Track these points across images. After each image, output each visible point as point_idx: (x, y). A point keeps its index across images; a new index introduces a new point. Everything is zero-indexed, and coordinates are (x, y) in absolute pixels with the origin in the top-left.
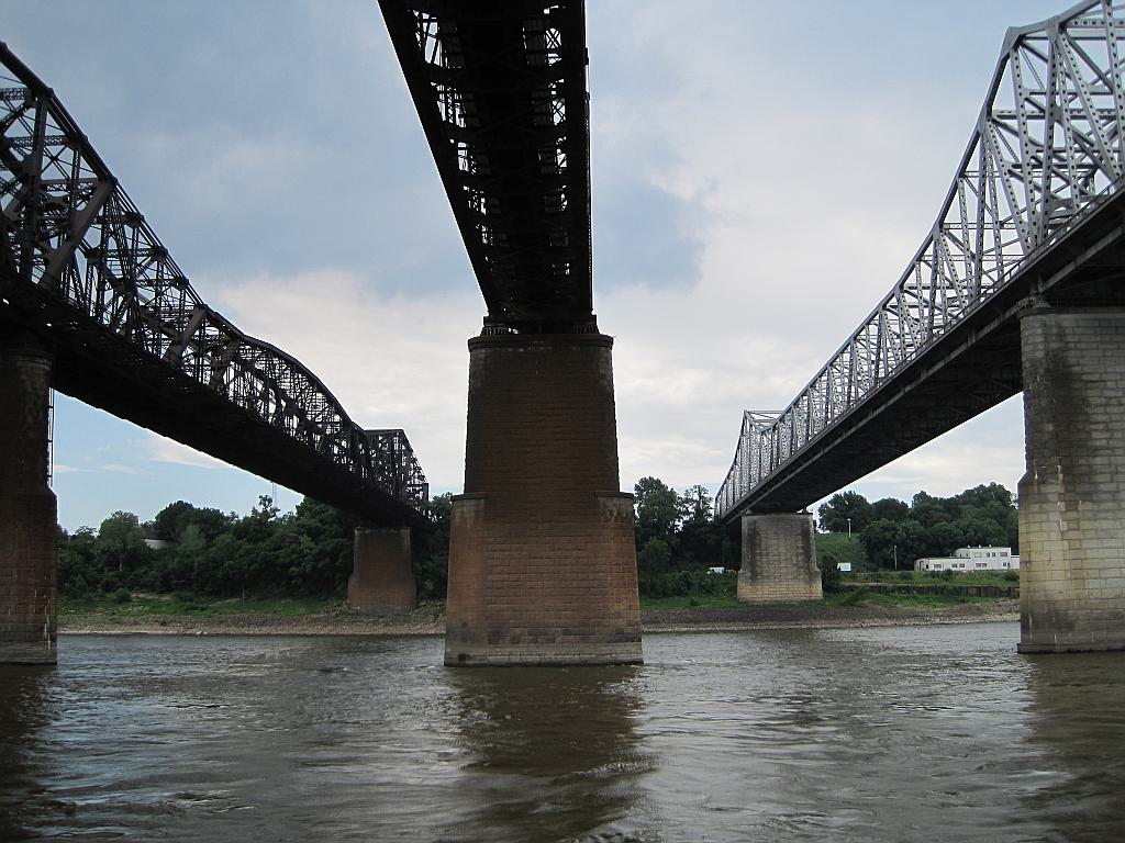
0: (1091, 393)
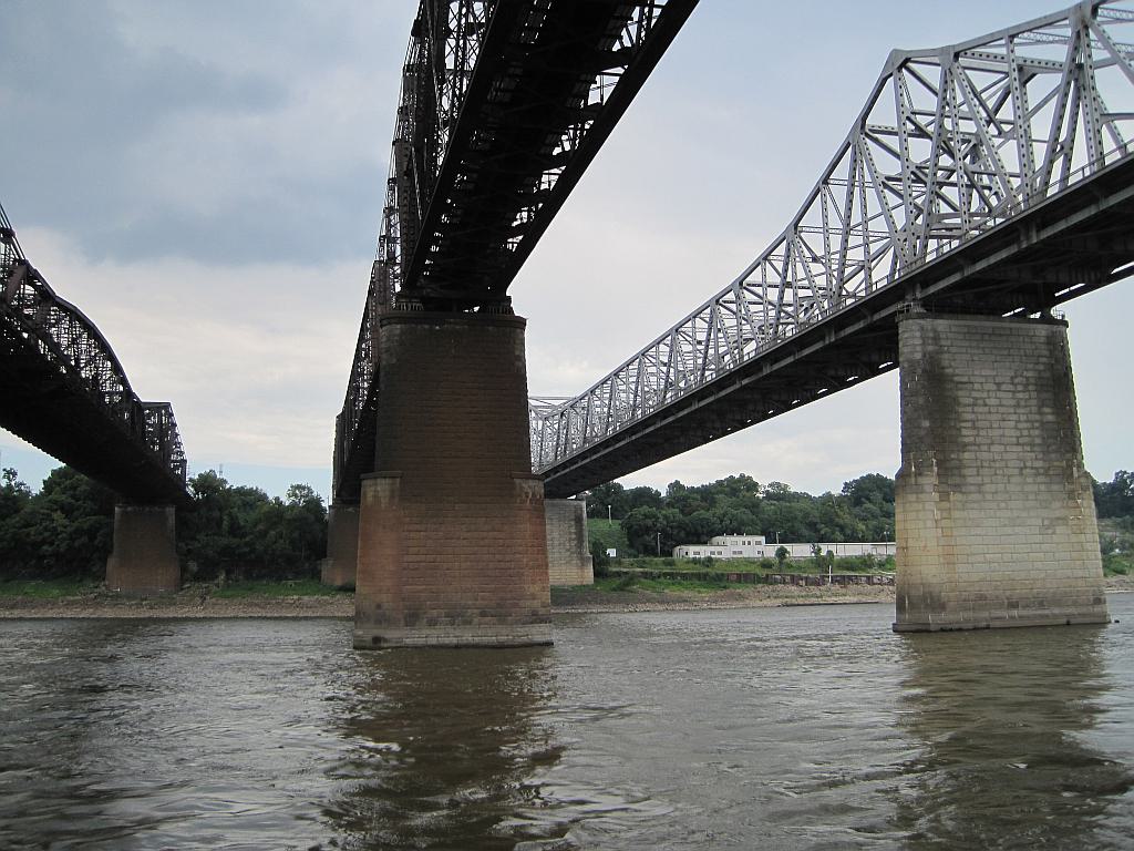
0: (960, 393)
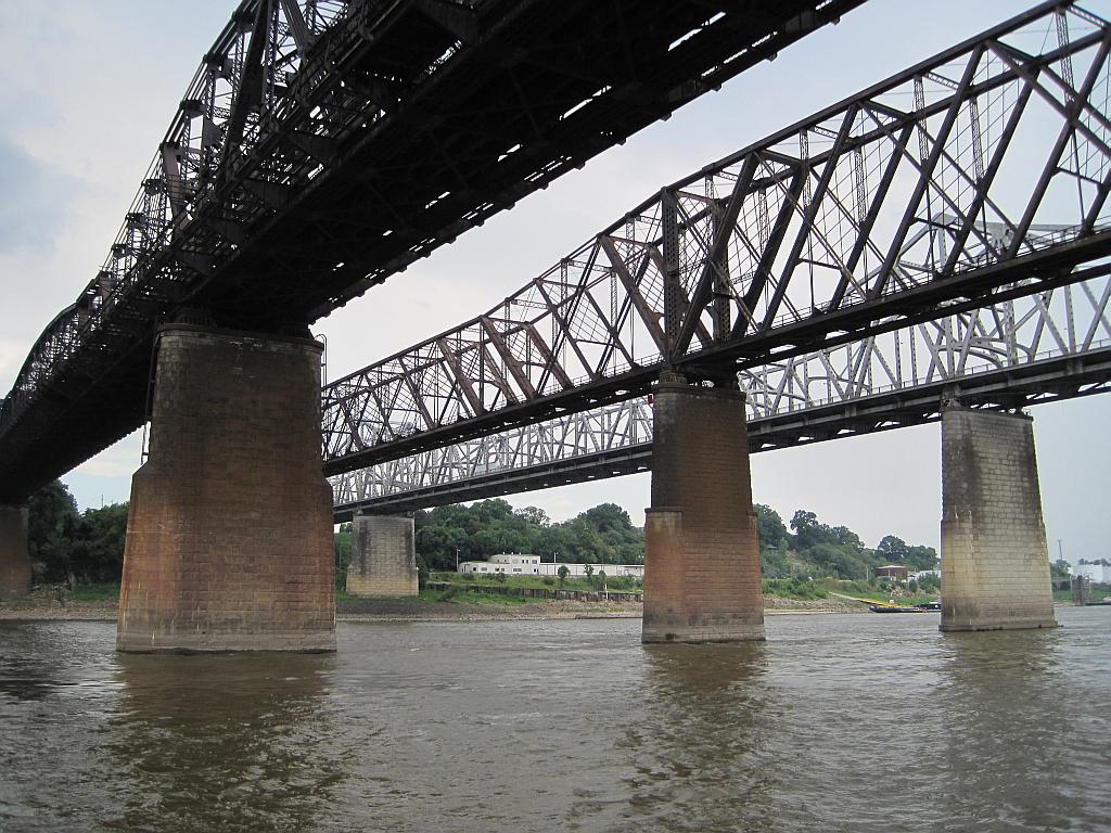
0: (982, 465)
